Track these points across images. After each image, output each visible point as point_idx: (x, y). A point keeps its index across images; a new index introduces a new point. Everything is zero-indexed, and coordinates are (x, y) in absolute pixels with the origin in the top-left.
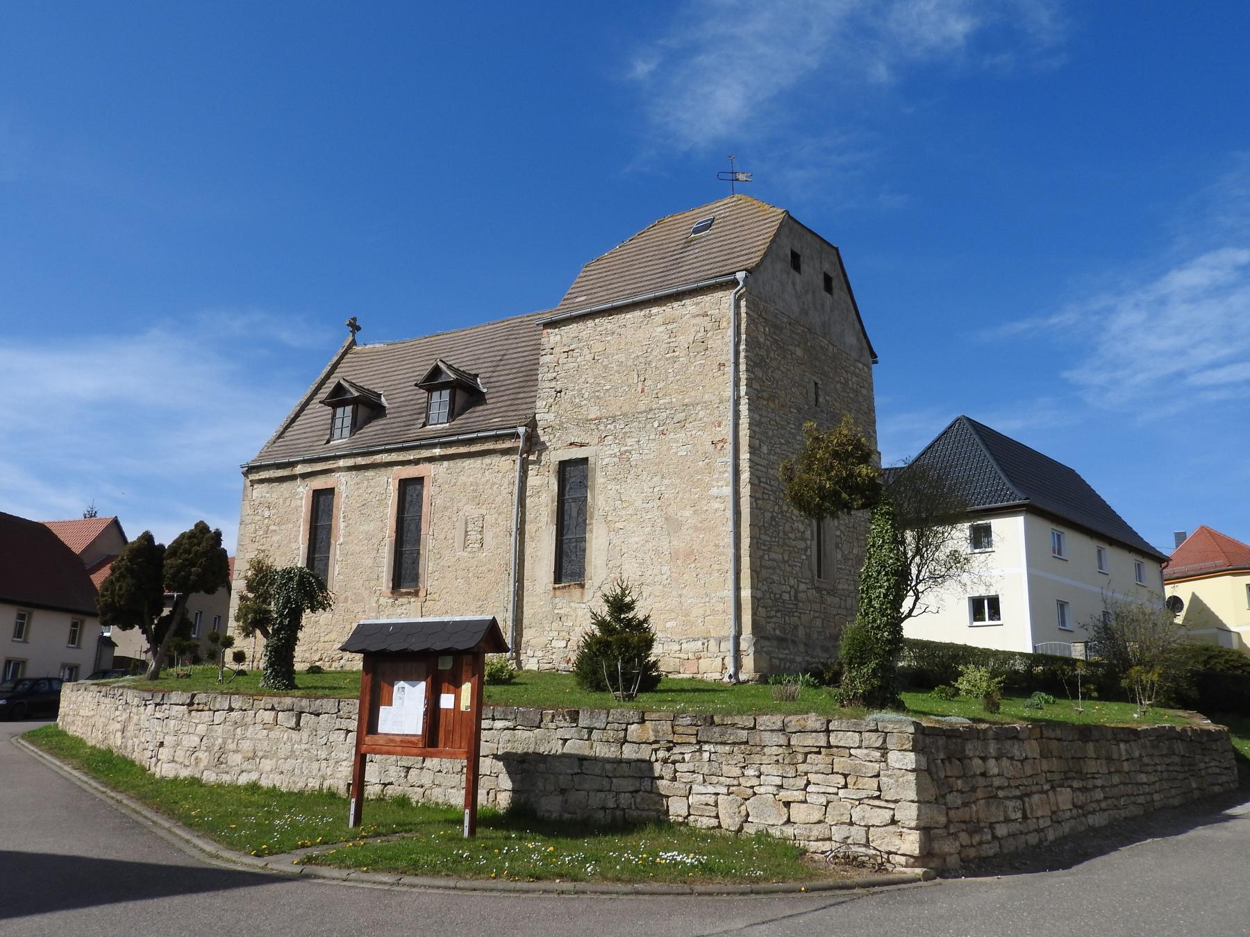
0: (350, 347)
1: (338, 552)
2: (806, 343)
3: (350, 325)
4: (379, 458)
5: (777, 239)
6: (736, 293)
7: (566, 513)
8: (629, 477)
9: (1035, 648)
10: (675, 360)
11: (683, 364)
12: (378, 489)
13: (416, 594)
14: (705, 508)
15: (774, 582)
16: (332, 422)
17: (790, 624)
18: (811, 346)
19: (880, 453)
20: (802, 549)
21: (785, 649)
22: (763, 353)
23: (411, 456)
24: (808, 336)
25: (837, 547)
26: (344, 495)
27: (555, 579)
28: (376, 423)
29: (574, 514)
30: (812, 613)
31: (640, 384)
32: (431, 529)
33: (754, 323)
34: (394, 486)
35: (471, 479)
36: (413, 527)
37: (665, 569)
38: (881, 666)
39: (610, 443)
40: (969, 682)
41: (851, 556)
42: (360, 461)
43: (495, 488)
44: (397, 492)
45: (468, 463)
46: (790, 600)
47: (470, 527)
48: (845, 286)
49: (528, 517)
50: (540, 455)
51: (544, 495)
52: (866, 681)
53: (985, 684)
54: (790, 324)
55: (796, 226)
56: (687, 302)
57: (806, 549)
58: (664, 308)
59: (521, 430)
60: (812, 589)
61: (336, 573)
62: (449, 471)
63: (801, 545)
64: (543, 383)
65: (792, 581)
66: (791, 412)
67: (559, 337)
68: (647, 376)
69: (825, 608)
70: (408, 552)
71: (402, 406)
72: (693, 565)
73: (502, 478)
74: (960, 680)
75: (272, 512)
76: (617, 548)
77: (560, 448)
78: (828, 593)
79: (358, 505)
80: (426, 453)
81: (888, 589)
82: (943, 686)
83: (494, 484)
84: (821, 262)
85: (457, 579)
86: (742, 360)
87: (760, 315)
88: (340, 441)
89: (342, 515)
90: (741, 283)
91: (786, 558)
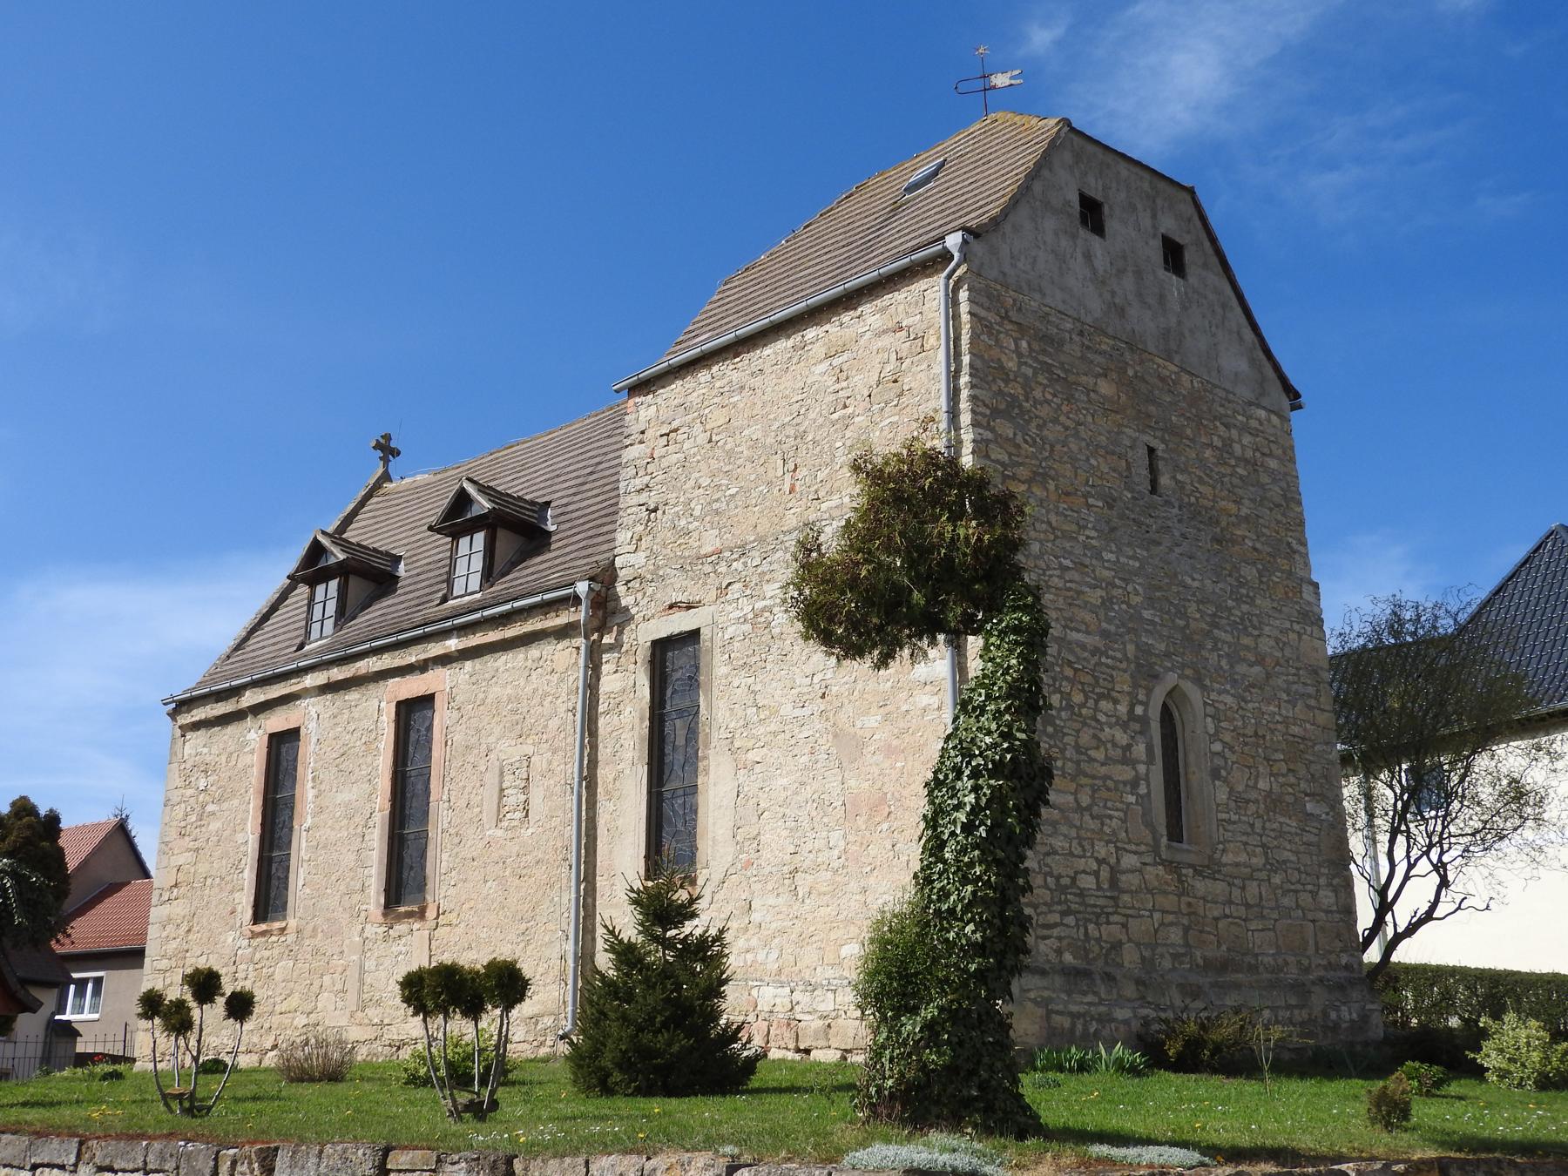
0: (377, 486)
1: (304, 844)
2: (1122, 371)
3: (378, 446)
5: (1045, 173)
6: (949, 277)
7: (667, 740)
8: (770, 658)
10: (847, 423)
11: (860, 428)
12: (367, 724)
13: (421, 914)
14: (904, 708)
15: (1056, 853)
16: (309, 608)
17: (1098, 940)
18: (1136, 376)
19: (1316, 586)
20: (1125, 783)
21: (1085, 993)
22: (1016, 389)
24: (1128, 356)
25: (1215, 774)
26: (314, 740)
27: (647, 870)
28: (377, 607)
29: (681, 741)
30: (1157, 916)
31: (788, 477)
32: (446, 789)
33: (990, 334)
35: (509, 691)
36: (420, 786)
37: (836, 836)
38: (951, 1014)
39: (736, 596)
40: (1501, 1051)
41: (1253, 795)
42: (337, 674)
43: (546, 703)
44: (392, 725)
45: (504, 660)
46: (1099, 888)
47: (508, 779)
48: (1215, 260)
49: (604, 753)
50: (620, 633)
51: (628, 710)
52: (910, 1055)
53: (1536, 1056)
54: (1081, 334)
55: (1091, 148)
56: (866, 308)
57: (1134, 784)
58: (827, 327)
59: (582, 588)
60: (1155, 864)
61: (301, 883)
62: (474, 679)
63: (1124, 773)
64: (628, 498)
65: (1102, 850)
66: (1089, 506)
67: (653, 408)
68: (799, 460)
69: (1189, 904)
70: (412, 837)
71: (423, 573)
72: (885, 826)
73: (558, 683)
74: (1487, 1046)
75: (211, 779)
76: (751, 802)
77: (653, 616)
78: (1198, 873)
79: (334, 756)
80: (435, 649)
81: (976, 810)
82: (1417, 1064)
83: (546, 694)
84: (1154, 216)
85: (486, 882)
86: (964, 405)
87: (1006, 317)
88: (319, 642)
89: (310, 777)
90: (956, 256)
91: (1085, 800)
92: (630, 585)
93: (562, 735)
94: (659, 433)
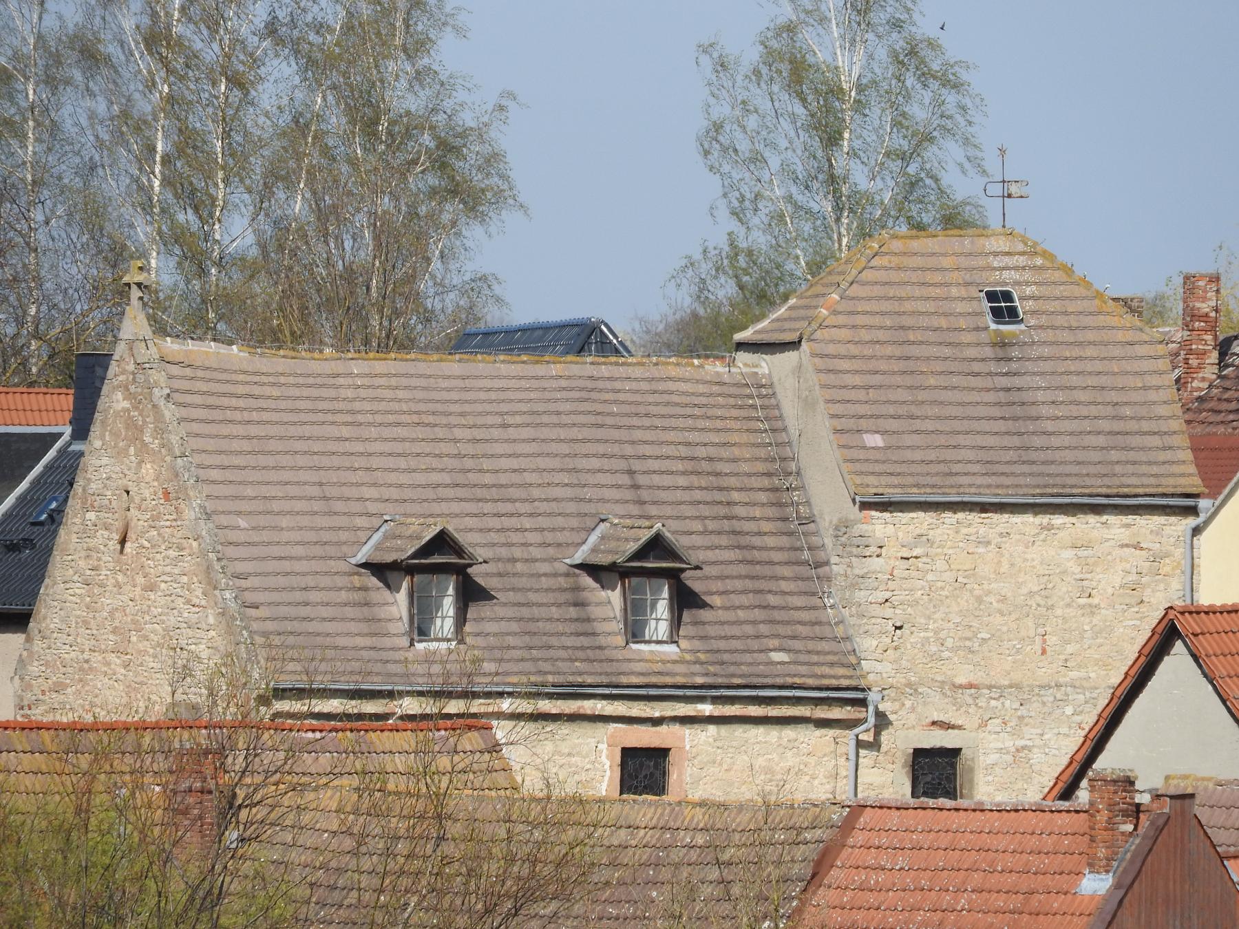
4: (588, 706)
9: (485, 742)
23: (656, 710)
34: (610, 757)
62: (719, 744)
92: (885, 692)
93: (405, 882)
94: (900, 555)
